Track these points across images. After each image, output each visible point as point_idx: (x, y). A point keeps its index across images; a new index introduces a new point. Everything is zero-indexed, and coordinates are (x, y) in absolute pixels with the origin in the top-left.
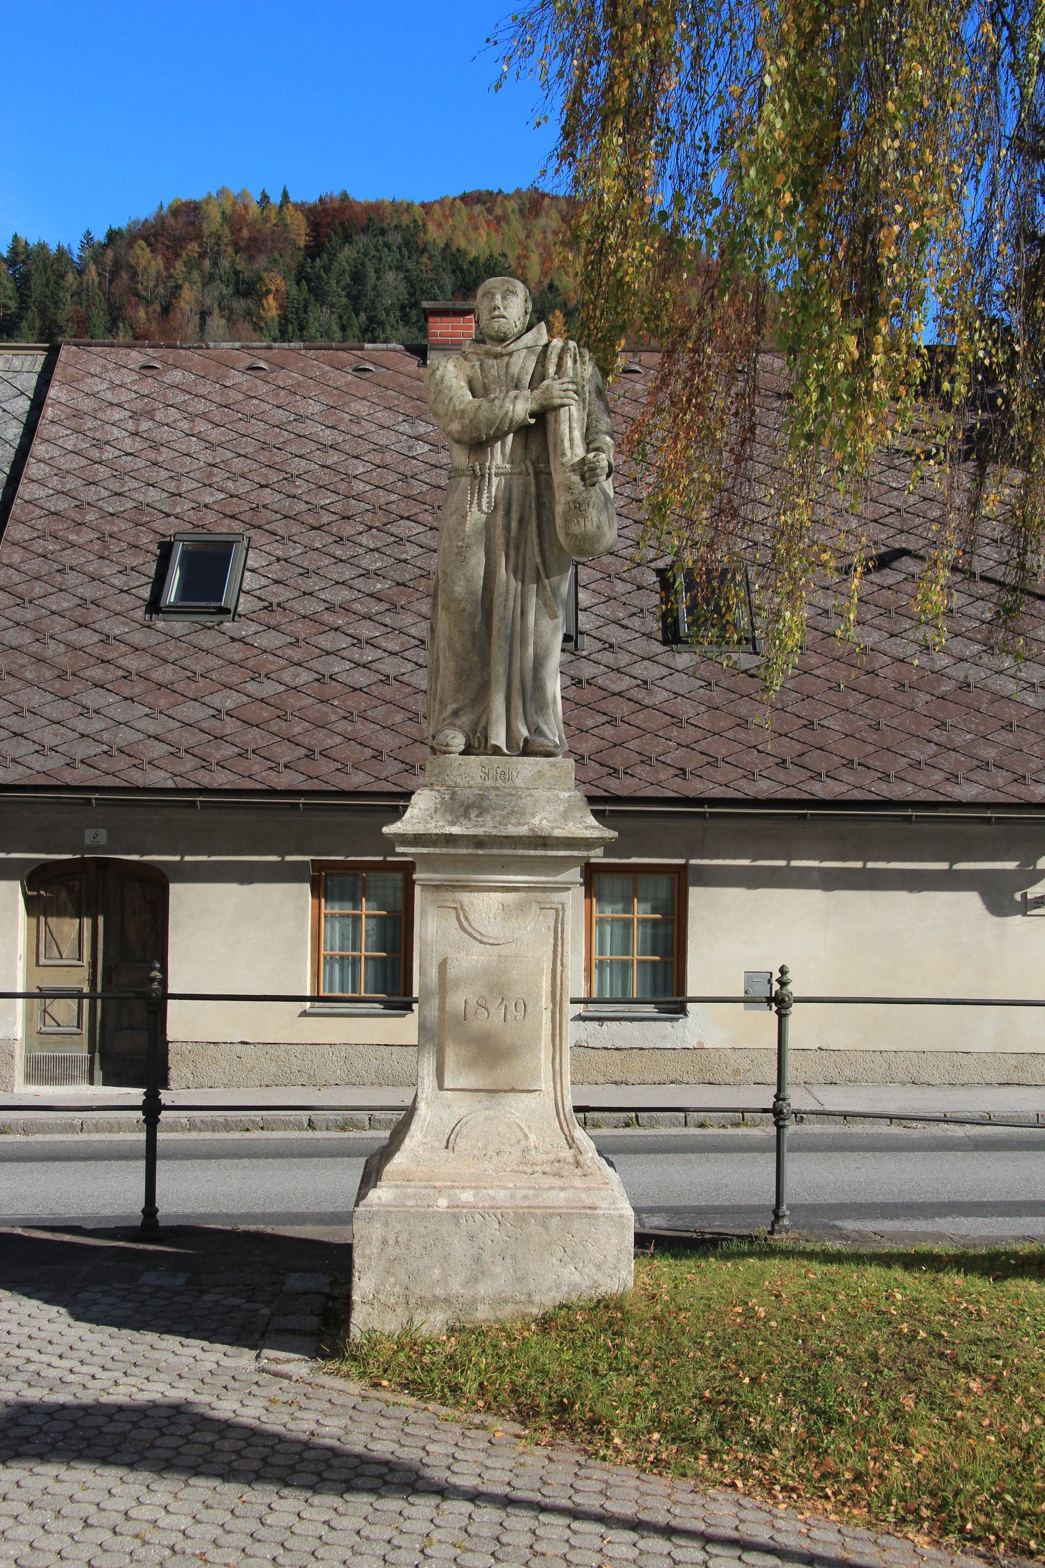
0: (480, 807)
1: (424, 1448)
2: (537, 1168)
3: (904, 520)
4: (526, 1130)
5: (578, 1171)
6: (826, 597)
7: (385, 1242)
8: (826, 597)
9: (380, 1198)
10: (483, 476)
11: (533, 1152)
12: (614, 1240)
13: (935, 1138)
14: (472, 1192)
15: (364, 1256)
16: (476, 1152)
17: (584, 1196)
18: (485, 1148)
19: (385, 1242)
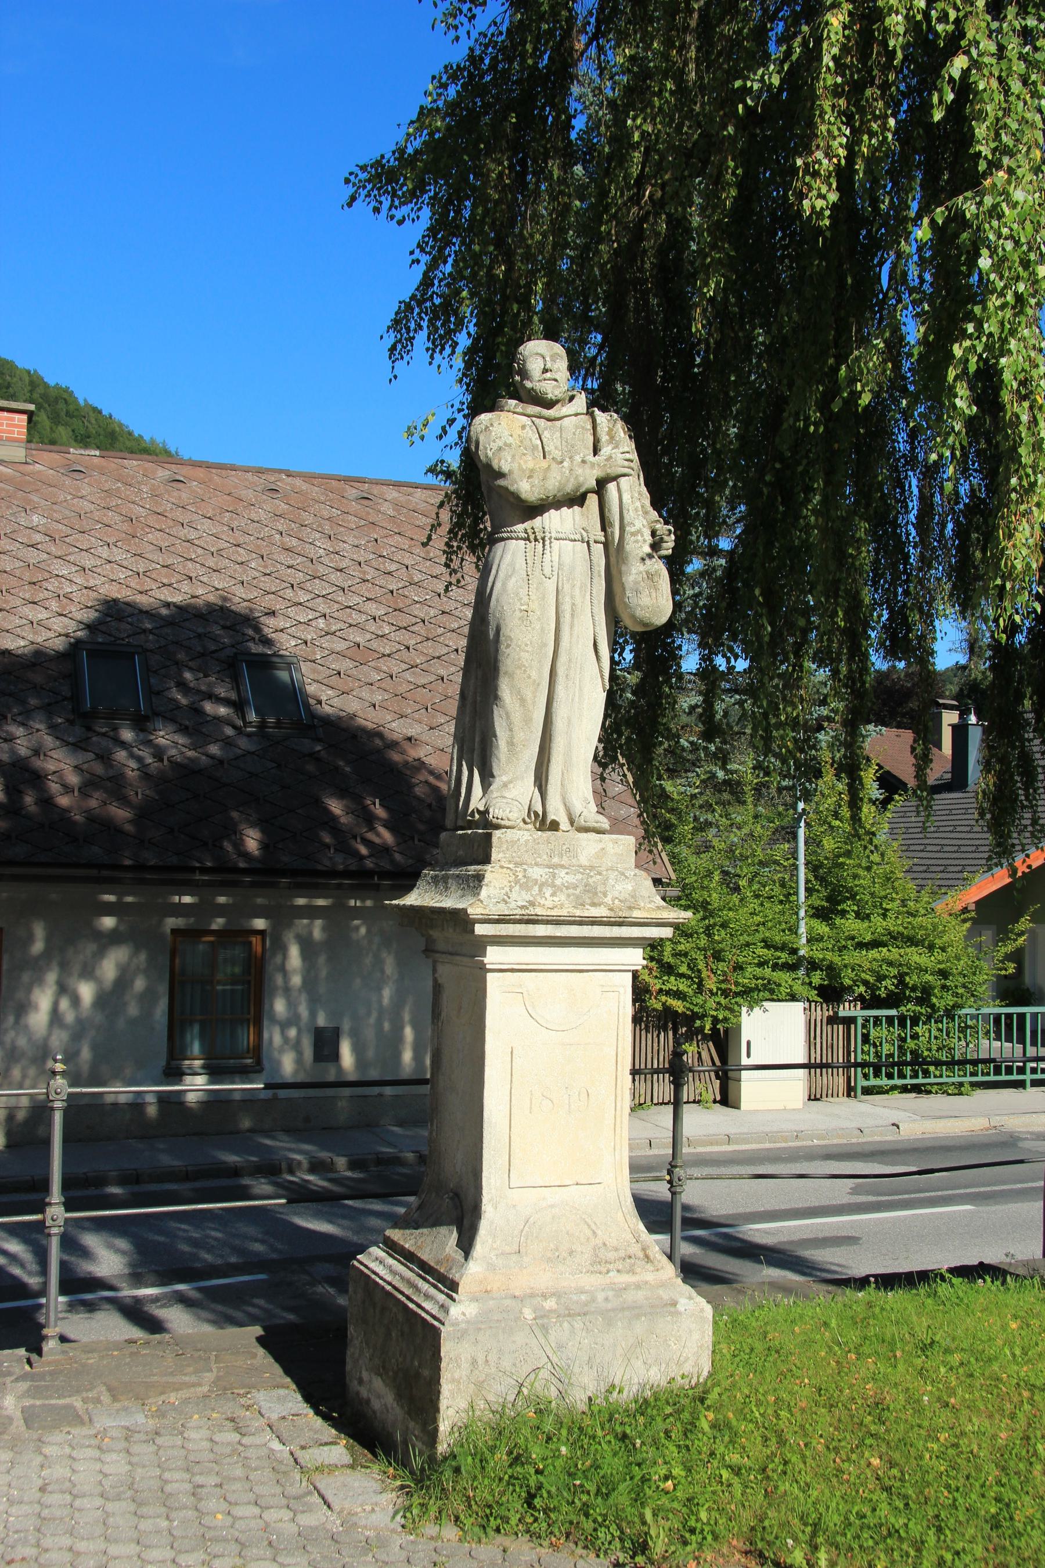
0: (553, 885)
1: (71, 1549)
2: (611, 1267)
3: (428, 630)
4: (593, 1227)
5: (649, 1266)
6: (372, 692)
7: (474, 1362)
8: (372, 692)
9: (464, 1314)
10: (543, 539)
11: (603, 1250)
12: (696, 1336)
13: (996, 1204)
14: (554, 1299)
15: (453, 1380)
16: (549, 1254)
17: (661, 1292)
18: (557, 1250)
19: (474, 1362)
